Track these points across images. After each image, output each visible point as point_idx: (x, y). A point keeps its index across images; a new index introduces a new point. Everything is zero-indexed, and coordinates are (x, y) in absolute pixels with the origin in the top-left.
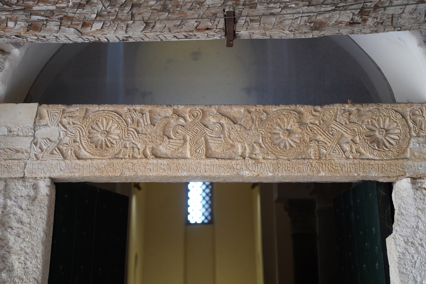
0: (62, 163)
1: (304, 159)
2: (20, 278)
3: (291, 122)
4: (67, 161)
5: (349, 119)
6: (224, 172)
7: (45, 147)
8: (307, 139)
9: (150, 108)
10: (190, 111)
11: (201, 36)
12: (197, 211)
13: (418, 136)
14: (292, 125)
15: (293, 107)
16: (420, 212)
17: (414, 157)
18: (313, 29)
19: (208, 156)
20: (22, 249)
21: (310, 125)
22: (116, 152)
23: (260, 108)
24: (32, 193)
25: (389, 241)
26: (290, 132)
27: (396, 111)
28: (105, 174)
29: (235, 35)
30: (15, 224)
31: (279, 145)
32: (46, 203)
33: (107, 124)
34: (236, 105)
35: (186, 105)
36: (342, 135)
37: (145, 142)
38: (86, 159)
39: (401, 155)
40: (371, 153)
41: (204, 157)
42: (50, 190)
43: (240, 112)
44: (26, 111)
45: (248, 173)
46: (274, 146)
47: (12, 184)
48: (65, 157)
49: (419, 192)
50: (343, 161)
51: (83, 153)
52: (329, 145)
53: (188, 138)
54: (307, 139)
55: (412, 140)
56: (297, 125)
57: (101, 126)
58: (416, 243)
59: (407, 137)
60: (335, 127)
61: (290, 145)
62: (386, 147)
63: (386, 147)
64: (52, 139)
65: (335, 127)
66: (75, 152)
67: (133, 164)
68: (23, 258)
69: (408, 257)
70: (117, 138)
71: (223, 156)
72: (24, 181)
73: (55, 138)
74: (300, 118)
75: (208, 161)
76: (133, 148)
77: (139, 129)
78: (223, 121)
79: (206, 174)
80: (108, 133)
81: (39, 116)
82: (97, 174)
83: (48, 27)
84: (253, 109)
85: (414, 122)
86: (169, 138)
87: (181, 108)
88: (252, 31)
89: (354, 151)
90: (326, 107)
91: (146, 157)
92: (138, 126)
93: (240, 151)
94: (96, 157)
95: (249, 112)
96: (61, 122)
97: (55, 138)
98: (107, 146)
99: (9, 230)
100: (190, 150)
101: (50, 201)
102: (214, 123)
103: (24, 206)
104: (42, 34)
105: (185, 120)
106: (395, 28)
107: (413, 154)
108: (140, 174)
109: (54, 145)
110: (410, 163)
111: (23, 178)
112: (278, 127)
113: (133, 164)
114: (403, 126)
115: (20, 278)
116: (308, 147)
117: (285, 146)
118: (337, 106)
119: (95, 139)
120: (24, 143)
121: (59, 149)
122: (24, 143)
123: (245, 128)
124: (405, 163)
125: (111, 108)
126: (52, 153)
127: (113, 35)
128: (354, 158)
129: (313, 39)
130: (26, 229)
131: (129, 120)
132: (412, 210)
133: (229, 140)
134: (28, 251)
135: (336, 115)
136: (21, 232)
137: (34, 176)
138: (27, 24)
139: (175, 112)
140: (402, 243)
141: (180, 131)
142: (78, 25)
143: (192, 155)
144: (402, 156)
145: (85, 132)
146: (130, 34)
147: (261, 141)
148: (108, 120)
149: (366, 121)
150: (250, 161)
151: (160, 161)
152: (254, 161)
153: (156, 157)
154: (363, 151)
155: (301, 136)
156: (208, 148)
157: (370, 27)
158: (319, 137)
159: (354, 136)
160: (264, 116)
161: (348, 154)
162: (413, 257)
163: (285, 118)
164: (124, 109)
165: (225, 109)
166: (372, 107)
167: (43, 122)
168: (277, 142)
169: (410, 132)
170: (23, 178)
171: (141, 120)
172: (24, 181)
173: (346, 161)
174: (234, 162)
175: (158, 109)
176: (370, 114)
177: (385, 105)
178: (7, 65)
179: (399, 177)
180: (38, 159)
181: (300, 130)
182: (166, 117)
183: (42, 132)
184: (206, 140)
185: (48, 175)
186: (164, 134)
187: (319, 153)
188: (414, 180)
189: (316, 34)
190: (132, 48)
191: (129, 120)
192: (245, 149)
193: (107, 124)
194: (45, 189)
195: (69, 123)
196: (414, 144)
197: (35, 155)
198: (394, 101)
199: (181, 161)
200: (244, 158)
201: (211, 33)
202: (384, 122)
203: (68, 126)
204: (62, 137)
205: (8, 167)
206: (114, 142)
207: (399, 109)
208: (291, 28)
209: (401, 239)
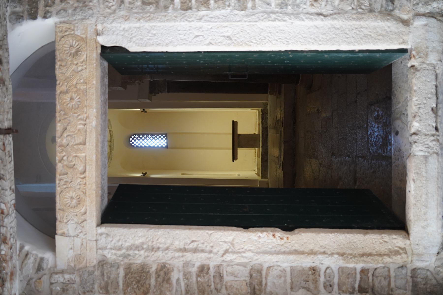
0: (88, 221)
1: (86, 92)
2: (147, 239)
3: (66, 98)
4: (87, 219)
5: (64, 66)
7: (80, 231)
8: (75, 89)
10: (60, 153)
13: (74, 30)
14: (67, 97)
15: (57, 96)
16: (115, 33)
19: (85, 144)
20: (133, 239)
21: (67, 87)
22: (82, 193)
24: (104, 236)
26: (72, 99)
27: (60, 40)
30: (120, 243)
31: (78, 105)
32: (109, 228)
33: (67, 198)
36: (73, 70)
37: (77, 178)
38: (86, 209)
39: (84, 40)
40: (83, 55)
41: (85, 146)
42: (103, 227)
43: (60, 126)
47: (99, 246)
49: (105, 33)
51: (83, 210)
52: (78, 78)
53: (75, 155)
54: (75, 89)
55: (76, 33)
56: (67, 95)
57: (68, 202)
58: (131, 37)
59: (74, 36)
61: (79, 98)
62: (80, 47)
63: (80, 47)
64: (75, 227)
66: (83, 215)
67: (89, 184)
68: (137, 238)
69: (137, 41)
70: (74, 193)
71: (84, 136)
72: (98, 240)
73: (75, 226)
74: (63, 93)
75: (87, 144)
76: (80, 184)
77: (70, 181)
78: (65, 135)
79: (95, 145)
80: (72, 198)
82: (94, 203)
83: (4, 233)
85: (66, 31)
86: (74, 165)
87: (57, 159)
88: (5, 119)
89: (82, 64)
90: (57, 78)
91: (85, 177)
92: (68, 182)
93: (82, 126)
94: (85, 204)
95: (60, 121)
96: (66, 223)
97: (75, 226)
98: (79, 198)
99: (123, 246)
100: (81, 153)
101: (108, 227)
102: (66, 140)
103: (111, 239)
104: (8, 236)
105: (65, 156)
106: (4, 39)
107: (84, 34)
108: (94, 180)
109: (79, 227)
110: (88, 36)
111: (96, 241)
112: (69, 105)
113: (89, 184)
114: (68, 37)
115: (147, 239)
117: (79, 102)
119: (75, 205)
120: (78, 241)
121: (81, 223)
122: (78, 241)
123: (69, 123)
124: (88, 38)
126: (83, 227)
128: (86, 65)
130: (122, 237)
131: (65, 187)
132: (114, 37)
133: (76, 132)
134: (133, 236)
135: (62, 73)
136: (124, 240)
137: (95, 235)
138: (3, 244)
139: (60, 161)
140: (131, 43)
141: (71, 159)
142: (2, 217)
143: (84, 153)
144: (85, 39)
145: (72, 210)
147: (76, 115)
148: (64, 199)
149: (65, 57)
150: (88, 121)
151: (87, 170)
152: (87, 119)
153: (85, 172)
154: (82, 60)
155: (73, 93)
157: (3, 53)
158: (74, 83)
159: (74, 64)
162: (138, 39)
166: (57, 53)
167: (66, 232)
168: (77, 106)
169: (72, 34)
170: (96, 241)
171: (65, 180)
172: (98, 240)
173: (87, 69)
174: (88, 130)
176: (61, 55)
177: (56, 47)
179: (97, 42)
180: (86, 234)
181: (70, 93)
182: (63, 167)
183: (72, 233)
184: (76, 145)
185: (95, 228)
186: (72, 168)
187: (83, 83)
188: (98, 34)
191: (65, 187)
192: (81, 124)
193: (67, 198)
194: (103, 229)
195: (67, 219)
196: (78, 33)
197: (84, 235)
199: (87, 158)
200: (86, 124)
201: (6, 142)
202: (66, 47)
203: (68, 219)
204: (74, 222)
206: (77, 194)
207: (59, 39)
208: (4, 96)
209: (129, 44)
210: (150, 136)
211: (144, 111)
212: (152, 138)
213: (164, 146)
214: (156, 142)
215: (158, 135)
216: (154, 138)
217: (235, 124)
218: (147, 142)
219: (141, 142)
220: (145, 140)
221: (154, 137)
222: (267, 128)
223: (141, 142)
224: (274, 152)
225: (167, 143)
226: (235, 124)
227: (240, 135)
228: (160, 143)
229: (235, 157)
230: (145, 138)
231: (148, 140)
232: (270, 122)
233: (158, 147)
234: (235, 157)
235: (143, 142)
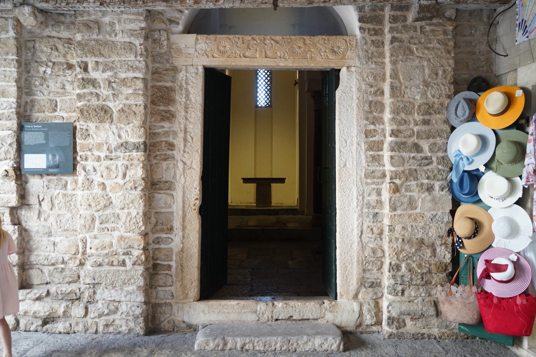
6: (271, 63)
8: (307, 50)
9: (242, 36)
11: (264, 6)
12: (262, 98)
14: (301, 44)
15: (301, 37)
17: (349, 58)
18: (309, 4)
19: (266, 57)
23: (288, 37)
24: (196, 71)
25: (337, 92)
26: (300, 47)
28: (224, 64)
29: (277, 6)
30: (191, 83)
34: (278, 35)
35: (257, 35)
38: (216, 58)
39: (343, 58)
44: (192, 37)
45: (282, 64)
46: (293, 53)
48: (208, 57)
50: (321, 60)
51: (215, 55)
54: (307, 50)
59: (347, 50)
60: (318, 45)
65: (318, 45)
73: (204, 49)
75: (266, 59)
78: (272, 42)
80: (225, 47)
81: (197, 39)
82: (221, 64)
84: (285, 37)
85: (350, 44)
93: (279, 55)
97: (204, 49)
104: (200, 5)
107: (348, 57)
110: (347, 61)
116: (307, 54)
118: (320, 37)
120: (192, 51)
122: (192, 51)
124: (345, 61)
125: (226, 36)
127: (227, 6)
129: (309, 8)
132: (346, 80)
139: (253, 38)
145: (216, 47)
146: (235, 5)
148: (225, 41)
153: (245, 57)
156: (266, 54)
158: (312, 50)
160: (289, 40)
161: (323, 57)
163: (298, 41)
164: (231, 37)
165: (273, 37)
167: (199, 42)
175: (62, 122)
178: (183, 17)
179: (342, 66)
183: (198, 46)
184: (265, 50)
188: (348, 67)
189: (310, 6)
190: (232, 9)
194: (201, 70)
196: (349, 53)
198: (347, 35)
199: (255, 59)
201: (267, 5)
205: (186, 61)
207: (345, 38)
210: (269, 88)
211: (296, 83)
212: (266, 90)
213: (258, 103)
214: (262, 95)
215: (270, 97)
216: (266, 92)
217: (281, 181)
218: (262, 85)
219: (262, 78)
220: (264, 83)
221: (268, 92)
222: (278, 214)
223: (262, 78)
224: (252, 221)
225: (262, 107)
226: (281, 181)
227: (270, 186)
228: (262, 99)
229: (246, 180)
230: (266, 83)
231: (264, 85)
232: (284, 217)
233: (257, 97)
234: (246, 180)
235: (262, 81)
